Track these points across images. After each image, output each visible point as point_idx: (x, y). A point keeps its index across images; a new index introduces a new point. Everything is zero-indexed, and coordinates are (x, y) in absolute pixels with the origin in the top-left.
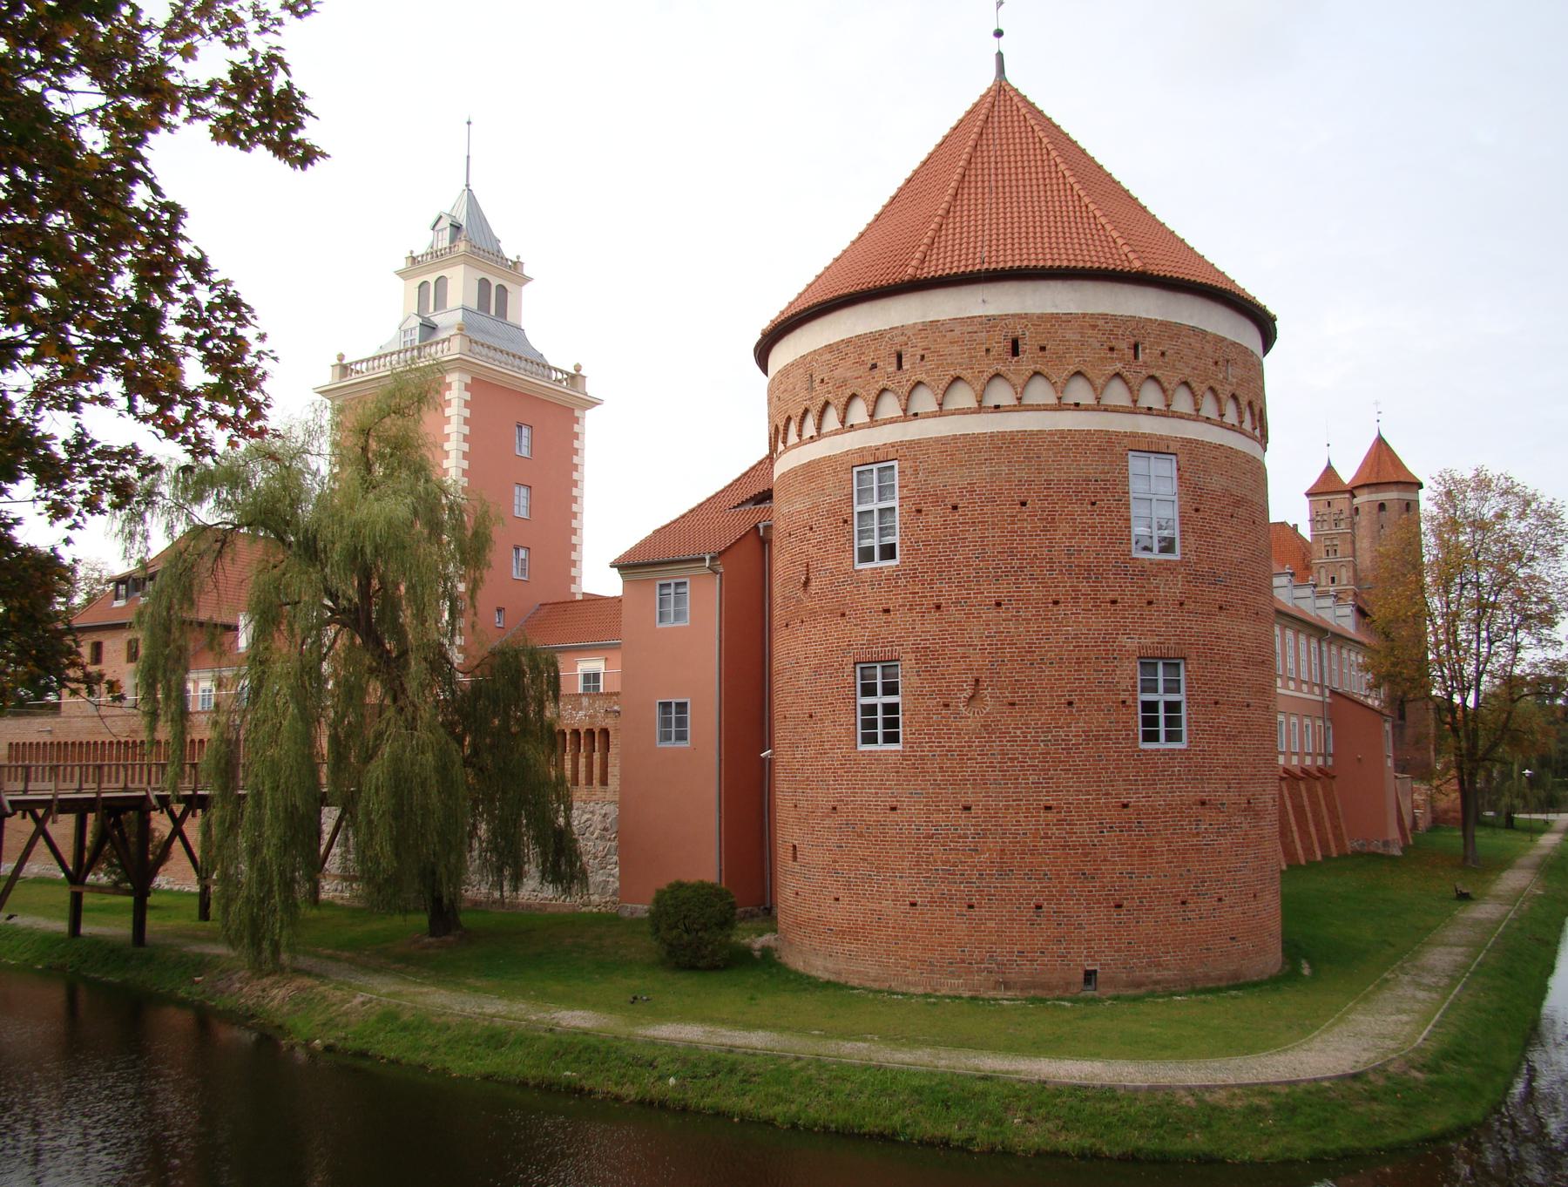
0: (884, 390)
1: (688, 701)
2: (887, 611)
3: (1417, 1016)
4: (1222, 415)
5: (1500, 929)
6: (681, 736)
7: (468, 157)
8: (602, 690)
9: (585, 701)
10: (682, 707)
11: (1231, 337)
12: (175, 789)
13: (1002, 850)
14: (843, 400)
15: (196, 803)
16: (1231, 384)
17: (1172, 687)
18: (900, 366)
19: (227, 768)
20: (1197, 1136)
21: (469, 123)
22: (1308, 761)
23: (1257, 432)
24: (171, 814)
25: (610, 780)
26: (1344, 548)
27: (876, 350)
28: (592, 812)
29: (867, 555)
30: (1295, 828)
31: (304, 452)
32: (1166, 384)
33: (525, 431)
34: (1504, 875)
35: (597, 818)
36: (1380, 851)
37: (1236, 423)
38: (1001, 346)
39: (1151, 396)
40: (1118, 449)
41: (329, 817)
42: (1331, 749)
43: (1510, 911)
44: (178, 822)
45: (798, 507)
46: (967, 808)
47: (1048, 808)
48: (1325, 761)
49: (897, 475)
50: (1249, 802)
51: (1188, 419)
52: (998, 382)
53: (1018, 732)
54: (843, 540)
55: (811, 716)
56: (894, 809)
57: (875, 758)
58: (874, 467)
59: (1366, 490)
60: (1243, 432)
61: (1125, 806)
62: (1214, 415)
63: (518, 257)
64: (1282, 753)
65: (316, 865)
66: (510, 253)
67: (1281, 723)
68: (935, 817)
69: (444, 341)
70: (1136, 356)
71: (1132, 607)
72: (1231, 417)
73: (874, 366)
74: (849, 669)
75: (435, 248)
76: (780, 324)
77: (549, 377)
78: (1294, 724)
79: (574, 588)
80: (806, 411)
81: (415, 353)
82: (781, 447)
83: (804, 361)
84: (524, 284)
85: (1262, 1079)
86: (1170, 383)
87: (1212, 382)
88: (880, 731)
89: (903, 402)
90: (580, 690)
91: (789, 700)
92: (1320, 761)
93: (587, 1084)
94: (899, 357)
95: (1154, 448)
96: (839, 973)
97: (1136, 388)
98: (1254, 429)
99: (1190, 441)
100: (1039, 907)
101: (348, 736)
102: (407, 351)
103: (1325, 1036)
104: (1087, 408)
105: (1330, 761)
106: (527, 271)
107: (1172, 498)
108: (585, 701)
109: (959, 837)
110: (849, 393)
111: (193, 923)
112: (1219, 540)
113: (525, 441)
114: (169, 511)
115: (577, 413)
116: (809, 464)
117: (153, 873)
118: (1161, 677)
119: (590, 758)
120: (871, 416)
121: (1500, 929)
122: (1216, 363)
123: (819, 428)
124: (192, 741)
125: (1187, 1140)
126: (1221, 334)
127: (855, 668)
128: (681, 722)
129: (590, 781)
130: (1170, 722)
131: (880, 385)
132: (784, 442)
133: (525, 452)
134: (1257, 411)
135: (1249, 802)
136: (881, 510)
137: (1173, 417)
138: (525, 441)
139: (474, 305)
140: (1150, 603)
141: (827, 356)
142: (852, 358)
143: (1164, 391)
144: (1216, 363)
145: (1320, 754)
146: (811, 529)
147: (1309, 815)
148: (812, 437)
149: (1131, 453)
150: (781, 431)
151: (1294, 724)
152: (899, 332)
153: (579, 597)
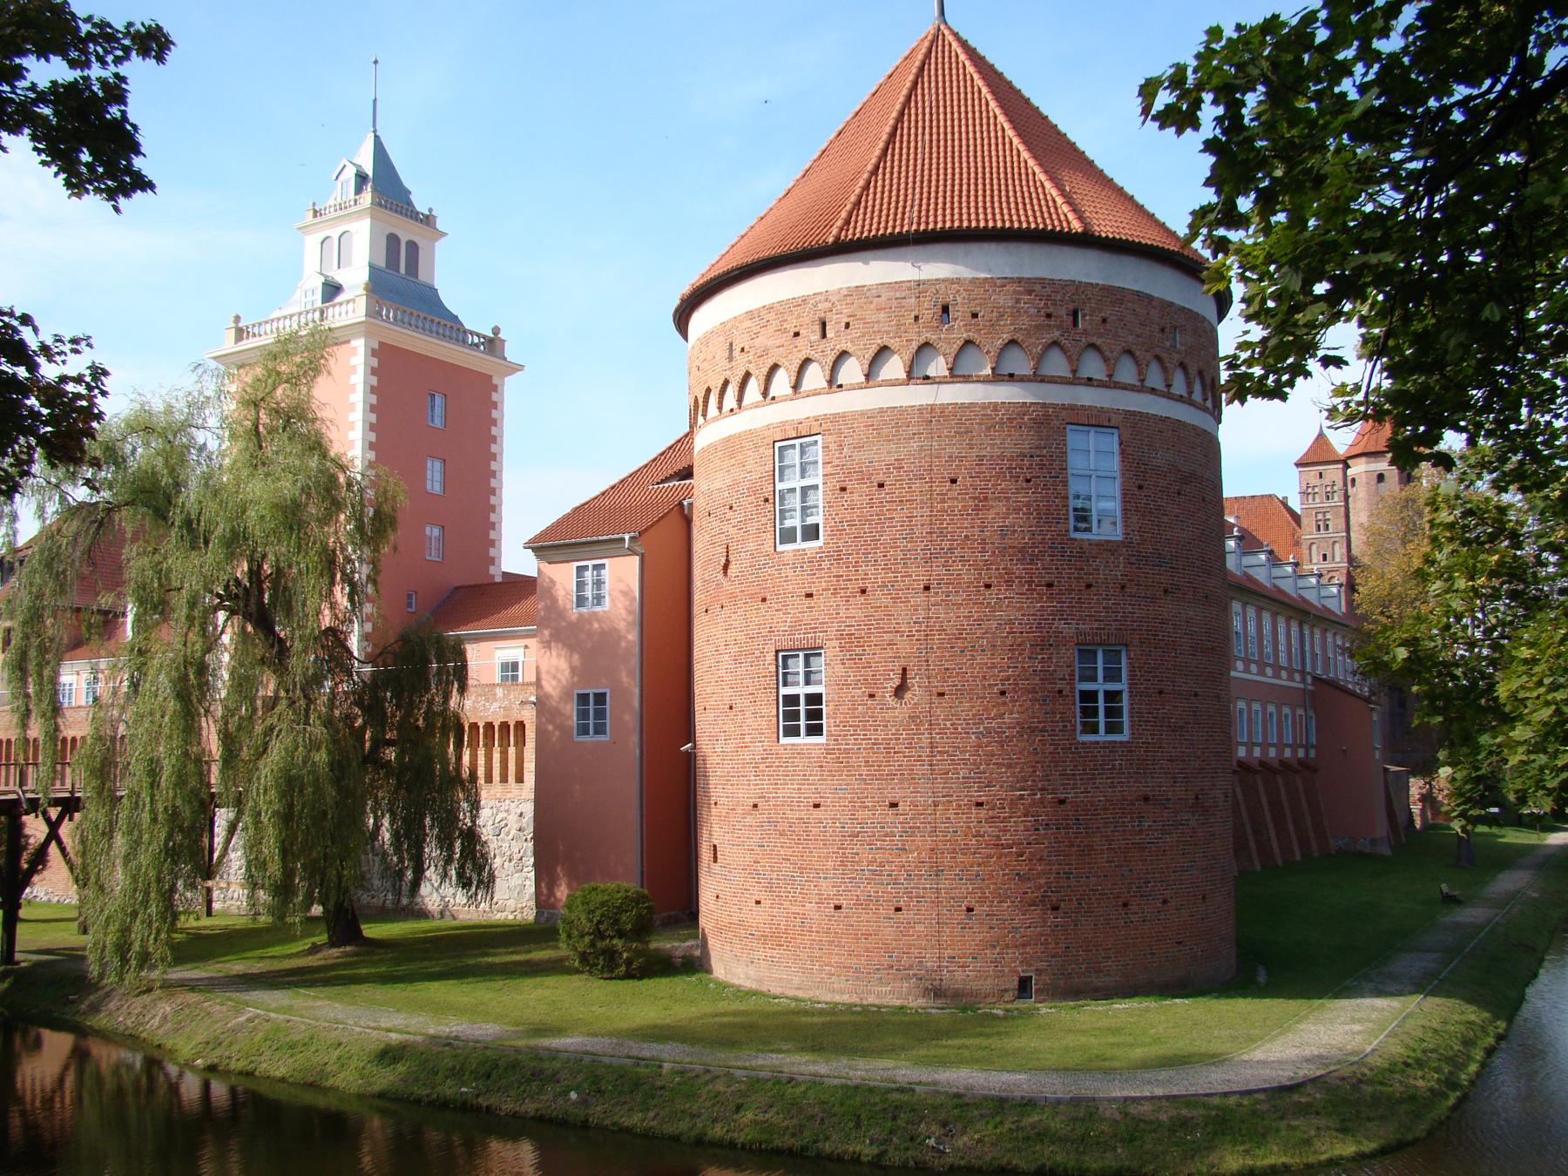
0: (927, 345)
1: (607, 691)
2: (809, 595)
3: (1370, 1025)
4: (1169, 386)
5: (1483, 934)
6: (600, 730)
7: (375, 101)
8: (520, 680)
9: (499, 692)
10: (601, 698)
11: (1179, 302)
12: (46, 793)
13: (933, 850)
14: (765, 370)
15: (70, 805)
16: (1179, 352)
17: (1113, 675)
18: (824, 336)
19: (105, 768)
20: (1119, 1151)
21: (376, 62)
22: (1287, 753)
23: (1209, 404)
24: (48, 820)
25: (525, 778)
26: (1336, 523)
27: (799, 317)
28: (507, 811)
29: (788, 536)
30: (1271, 826)
31: (190, 426)
32: (1107, 353)
33: (439, 400)
34: (1500, 876)
35: (513, 818)
36: (1367, 851)
37: (1185, 395)
38: (929, 312)
39: (1093, 366)
40: (1055, 423)
41: (223, 817)
42: (1313, 740)
43: (1496, 915)
44: (54, 826)
45: (718, 484)
46: (894, 805)
47: (979, 804)
48: (1307, 753)
49: (820, 450)
50: (1197, 798)
51: (1132, 390)
52: (971, 350)
53: (948, 723)
54: (764, 520)
55: (731, 708)
56: (817, 806)
57: (798, 752)
58: (797, 442)
59: (1363, 459)
60: (1191, 403)
61: (1062, 802)
62: (1160, 386)
63: (430, 210)
64: (1242, 744)
65: (207, 869)
66: (421, 206)
67: (1241, 711)
68: (860, 814)
69: (348, 302)
70: (1075, 324)
71: (1070, 591)
72: (1179, 387)
73: (797, 334)
74: (770, 657)
75: (339, 200)
76: (699, 288)
77: (464, 341)
78: (1286, 716)
79: (492, 570)
80: (726, 383)
81: (317, 315)
82: (701, 420)
83: (726, 328)
84: (436, 240)
85: (1192, 1091)
86: (1112, 352)
87: (1158, 351)
88: (802, 723)
89: (828, 372)
90: (498, 680)
91: (709, 690)
92: (1301, 753)
93: (483, 1101)
94: (824, 325)
95: (1096, 420)
96: (760, 981)
97: (1075, 357)
98: (1205, 400)
99: (1134, 413)
100: (970, 910)
101: (239, 728)
102: (308, 312)
103: (1268, 1046)
104: (1023, 379)
105: (1312, 753)
106: (440, 225)
107: (1114, 475)
108: (499, 692)
109: (886, 835)
110: (770, 363)
111: (73, 938)
112: (1165, 519)
113: (438, 411)
114: (40, 489)
115: (495, 381)
116: (728, 439)
117: (26, 880)
118: (1100, 665)
119: (504, 754)
120: (868, 376)
121: (1483, 934)
122: (1163, 330)
123: (740, 400)
124: (64, 740)
125: (1109, 1155)
126: (1169, 298)
127: (777, 656)
128: (600, 714)
129: (504, 779)
130: (1109, 712)
131: (802, 356)
132: (704, 415)
133: (438, 422)
134: (1208, 382)
135: (1197, 798)
136: (803, 488)
137: (1115, 387)
138: (438, 411)
139: (382, 263)
140: (1089, 586)
141: (748, 323)
142: (774, 325)
143: (1106, 360)
144: (1163, 330)
145: (1301, 746)
146: (731, 508)
147: (1288, 811)
148: (732, 410)
149: (1069, 427)
150: (701, 404)
151: (1286, 716)
152: (823, 298)
153: (498, 579)
